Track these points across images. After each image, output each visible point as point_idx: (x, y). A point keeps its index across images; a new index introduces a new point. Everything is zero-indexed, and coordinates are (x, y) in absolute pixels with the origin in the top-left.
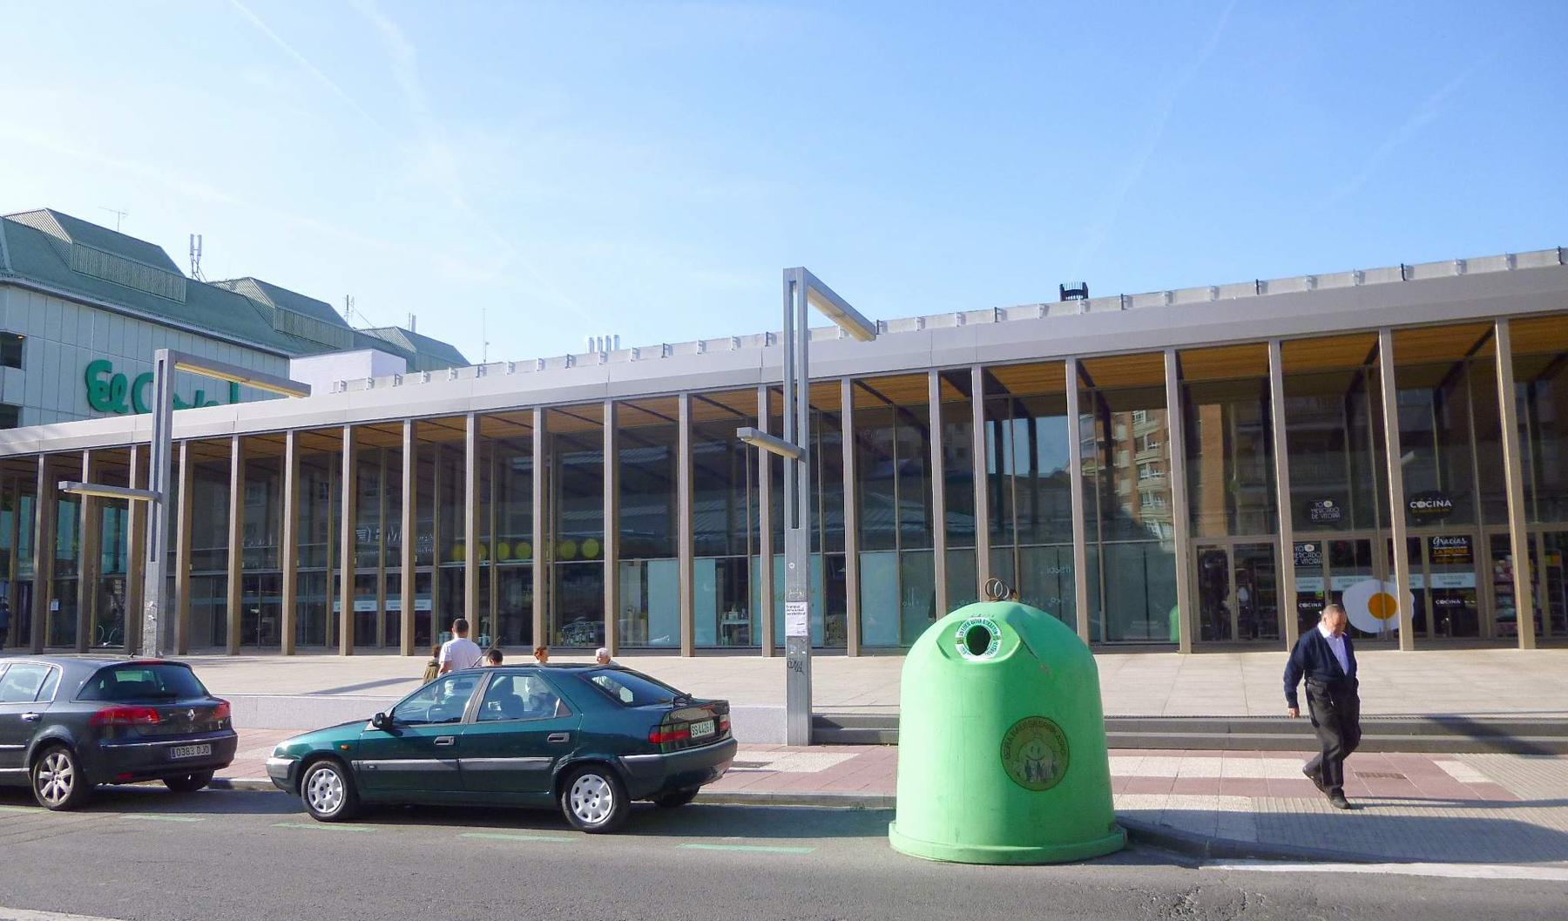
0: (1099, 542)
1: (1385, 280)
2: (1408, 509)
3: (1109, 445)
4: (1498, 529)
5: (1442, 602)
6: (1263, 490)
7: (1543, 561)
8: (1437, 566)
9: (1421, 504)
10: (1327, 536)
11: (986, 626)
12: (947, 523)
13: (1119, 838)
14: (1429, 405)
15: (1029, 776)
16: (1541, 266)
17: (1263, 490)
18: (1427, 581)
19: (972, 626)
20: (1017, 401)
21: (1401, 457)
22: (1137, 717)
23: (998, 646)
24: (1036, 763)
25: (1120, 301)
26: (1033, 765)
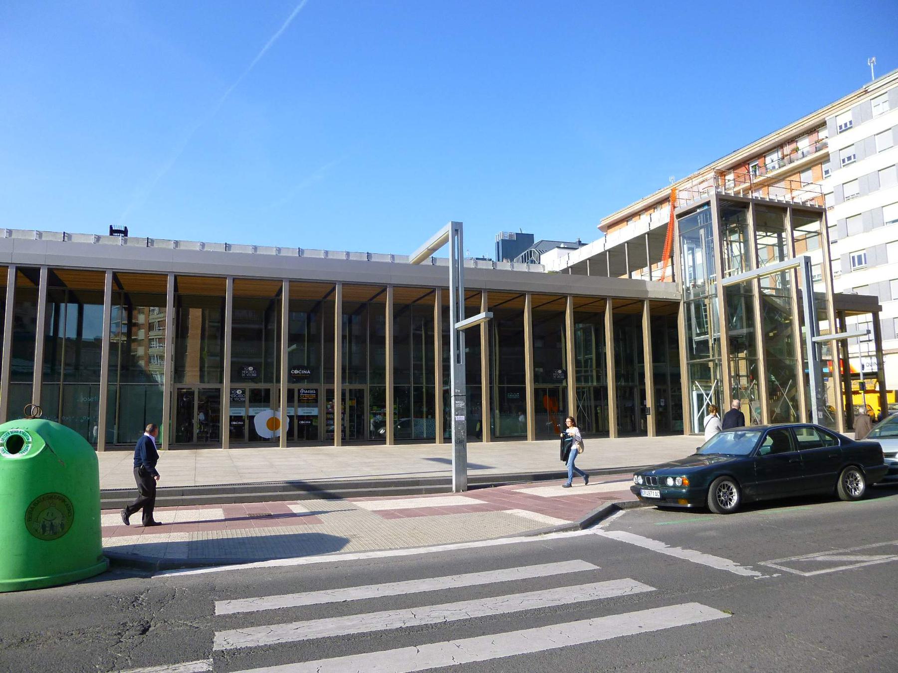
0: (61, 383)
1: (290, 254)
2: (290, 375)
3: (131, 325)
4: (329, 386)
5: (302, 422)
6: (218, 358)
7: (348, 403)
8: (301, 404)
9: (296, 372)
10: (249, 386)
11: (21, 435)
12: (11, 365)
13: (103, 565)
14: (304, 322)
15: (44, 531)
16: (360, 260)
17: (218, 358)
18: (296, 411)
19: (11, 435)
20: (71, 293)
21: (288, 347)
22: (128, 489)
23: (29, 448)
24: (50, 523)
25: (63, 235)
26: (48, 524)
